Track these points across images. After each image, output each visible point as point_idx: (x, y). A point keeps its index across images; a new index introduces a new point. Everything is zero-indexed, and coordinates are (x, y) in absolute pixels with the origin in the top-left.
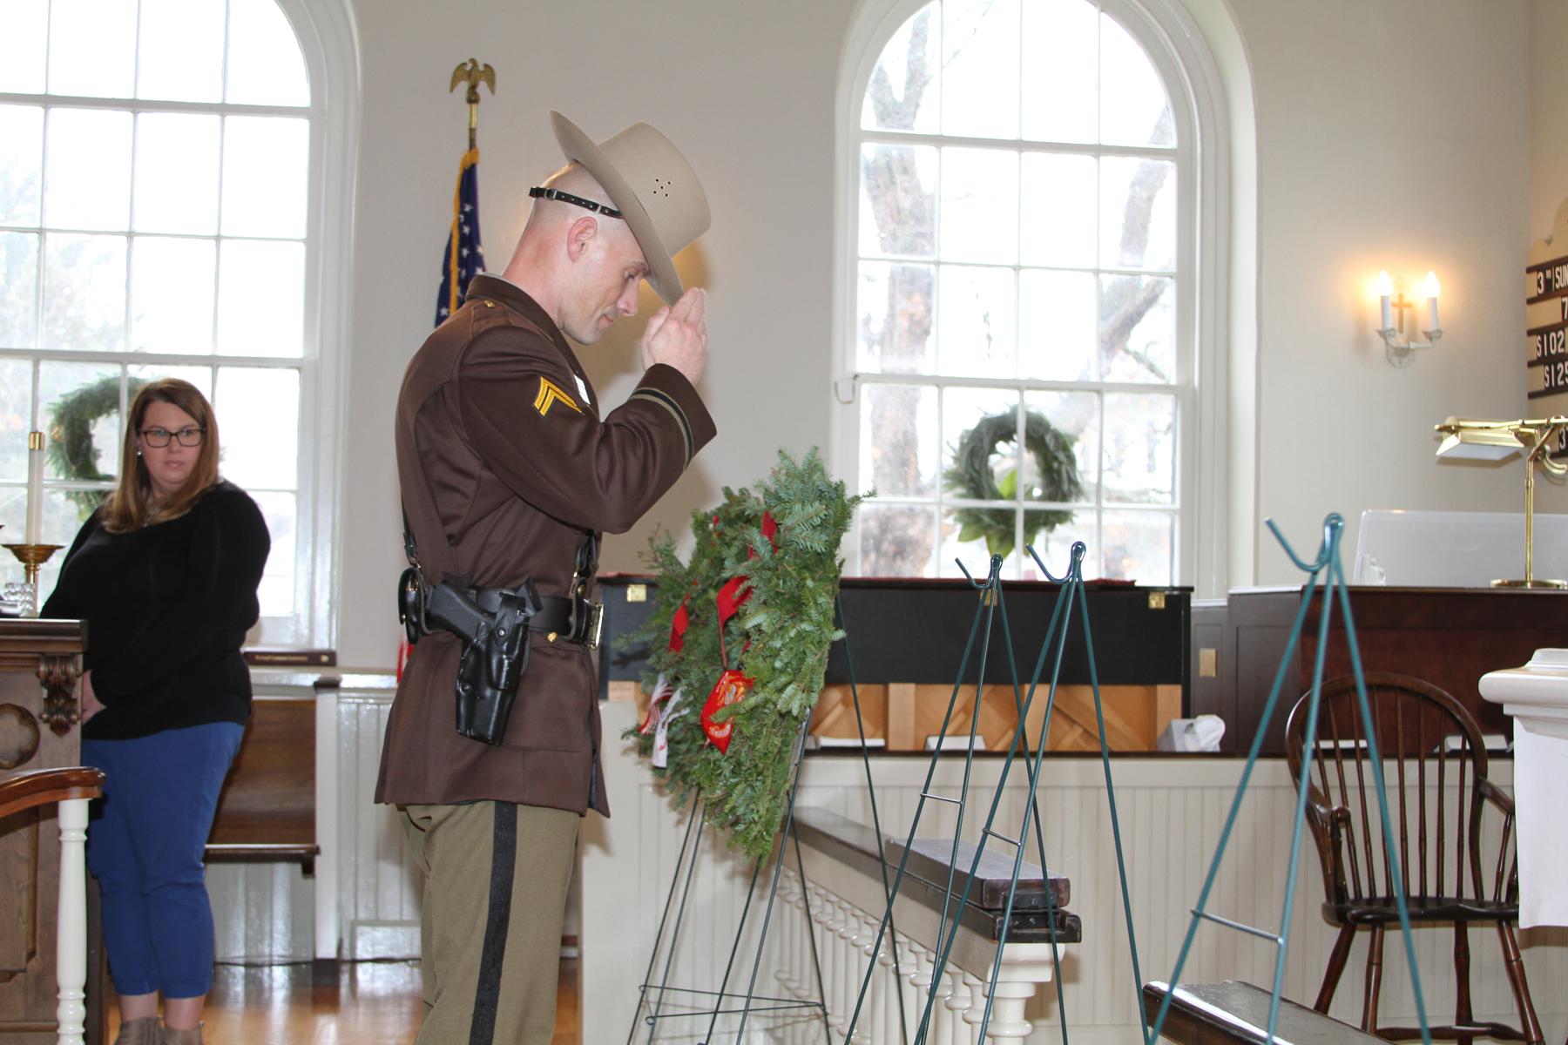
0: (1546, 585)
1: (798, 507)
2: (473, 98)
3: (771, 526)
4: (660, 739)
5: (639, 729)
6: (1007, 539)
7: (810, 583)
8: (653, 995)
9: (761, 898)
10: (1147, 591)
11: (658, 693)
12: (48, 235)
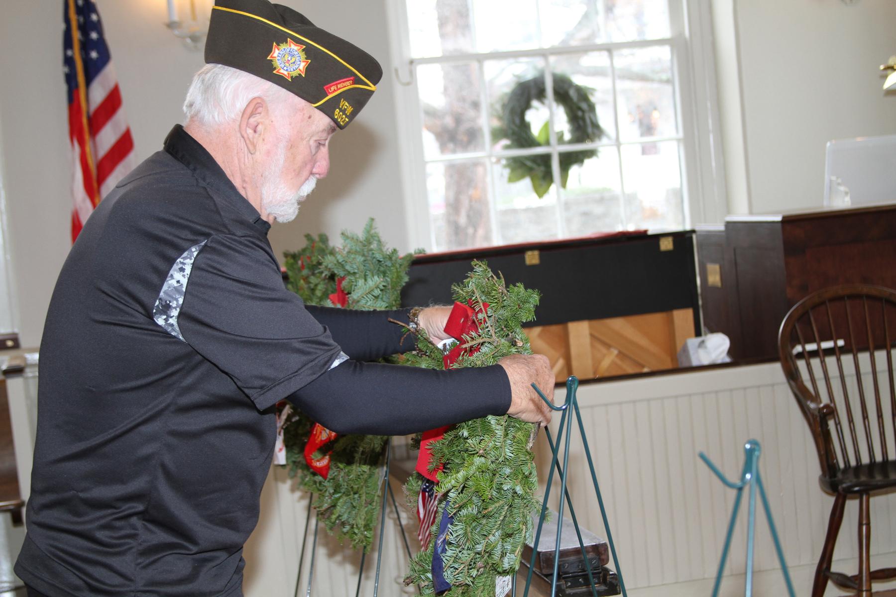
1: (361, 282)
6: (548, 177)
9: (367, 578)
10: (657, 237)
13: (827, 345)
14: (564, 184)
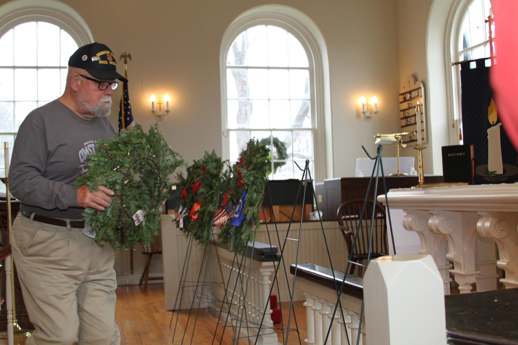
0: (403, 175)
1: (210, 164)
2: (126, 62)
3: (204, 169)
4: (181, 221)
5: (176, 219)
7: (214, 181)
8: (182, 283)
11: (180, 210)
12: (16, 103)
13: (352, 216)
14: (275, 173)
